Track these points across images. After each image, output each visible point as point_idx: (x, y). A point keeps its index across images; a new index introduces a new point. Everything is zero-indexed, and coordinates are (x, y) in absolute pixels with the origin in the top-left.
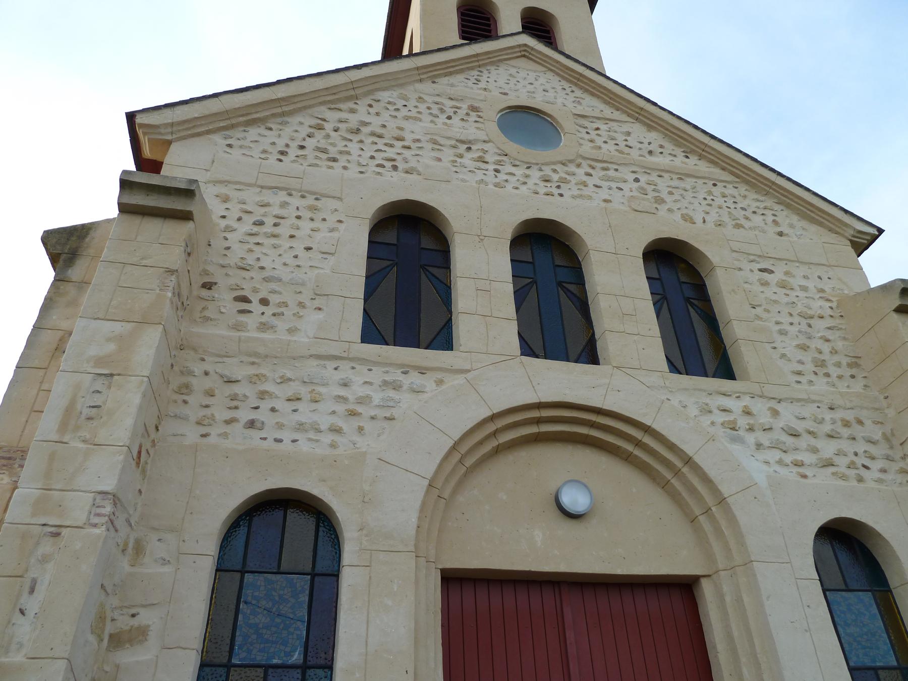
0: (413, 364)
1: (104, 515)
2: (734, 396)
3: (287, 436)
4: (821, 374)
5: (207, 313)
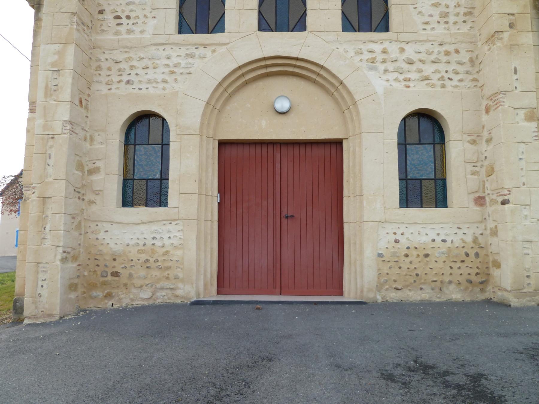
0: (200, 43)
1: (68, 130)
2: (379, 43)
3: (143, 86)
4: (442, 21)
5: (103, 28)
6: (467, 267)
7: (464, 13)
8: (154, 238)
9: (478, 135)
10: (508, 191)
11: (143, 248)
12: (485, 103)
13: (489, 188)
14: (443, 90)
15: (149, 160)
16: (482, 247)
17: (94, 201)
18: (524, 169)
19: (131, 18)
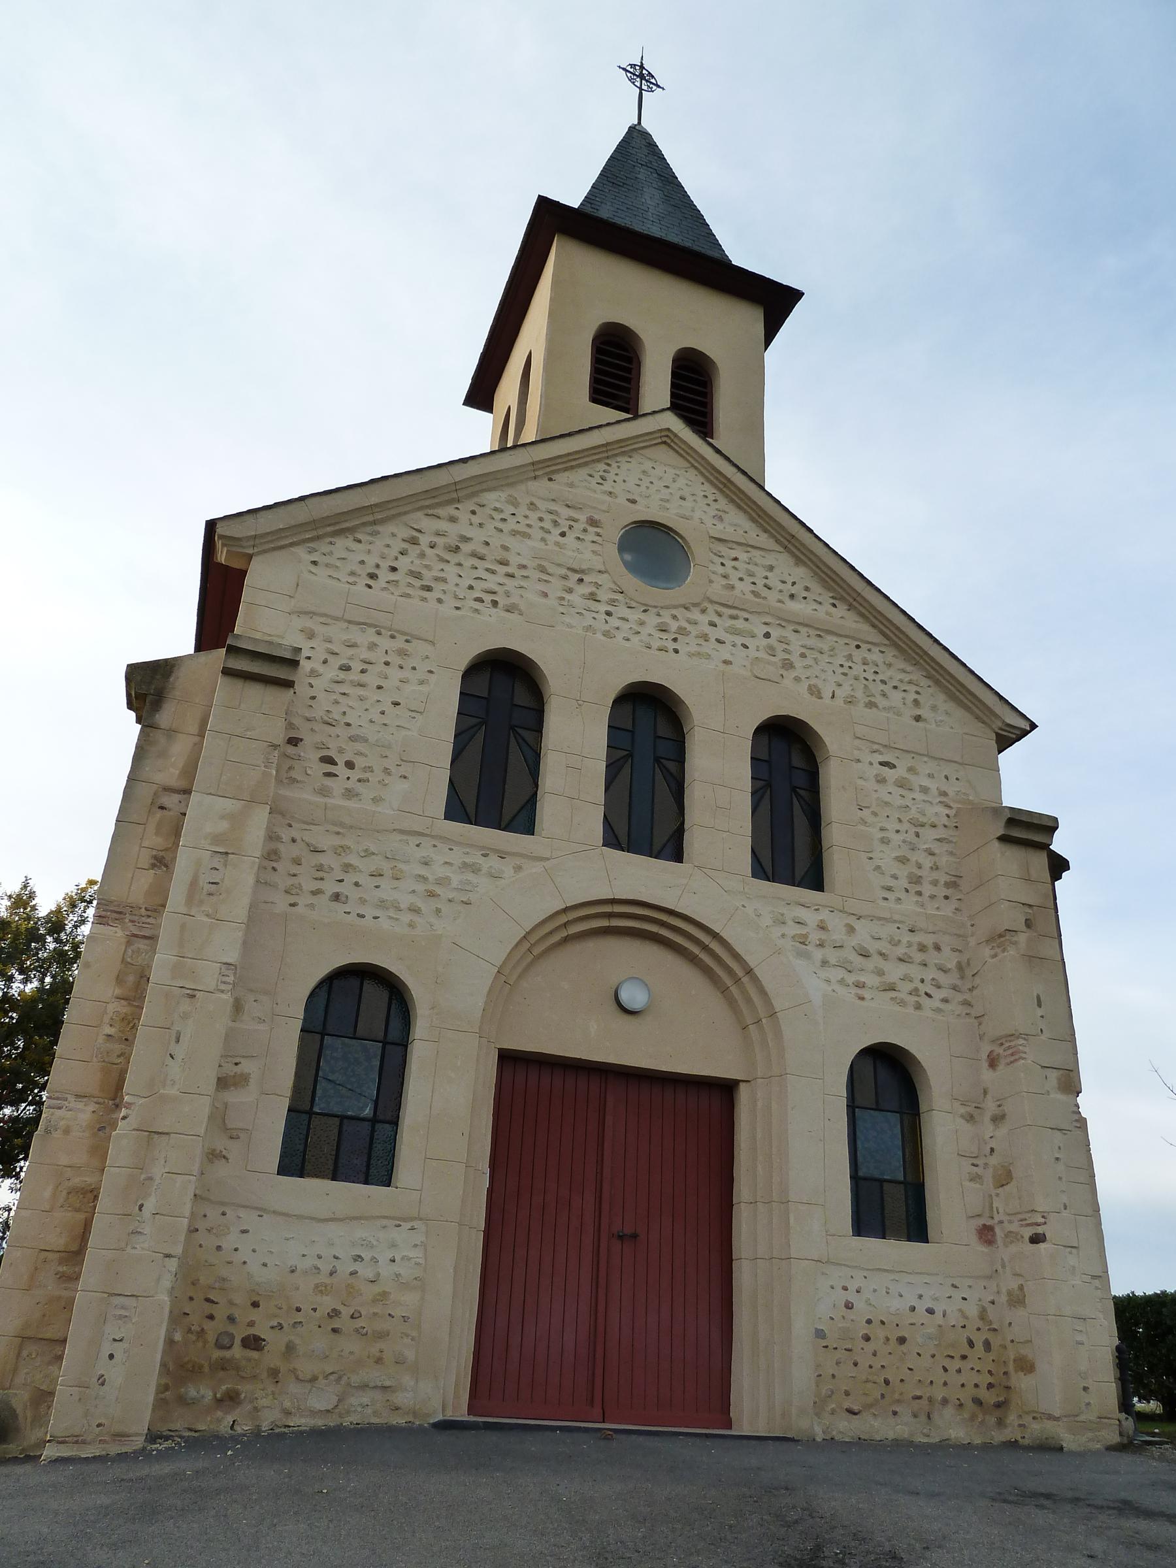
1: (229, 983)
3: (369, 912)
5: (294, 774)
6: (972, 1369)
7: (945, 881)
8: (358, 1258)
9: (977, 1105)
10: (1043, 1217)
11: (328, 1281)
12: (986, 1049)
13: (1001, 1210)
14: (918, 1013)
15: (351, 1074)
16: (995, 1330)
17: (224, 1153)
18: (1064, 1179)
19: (356, 768)
